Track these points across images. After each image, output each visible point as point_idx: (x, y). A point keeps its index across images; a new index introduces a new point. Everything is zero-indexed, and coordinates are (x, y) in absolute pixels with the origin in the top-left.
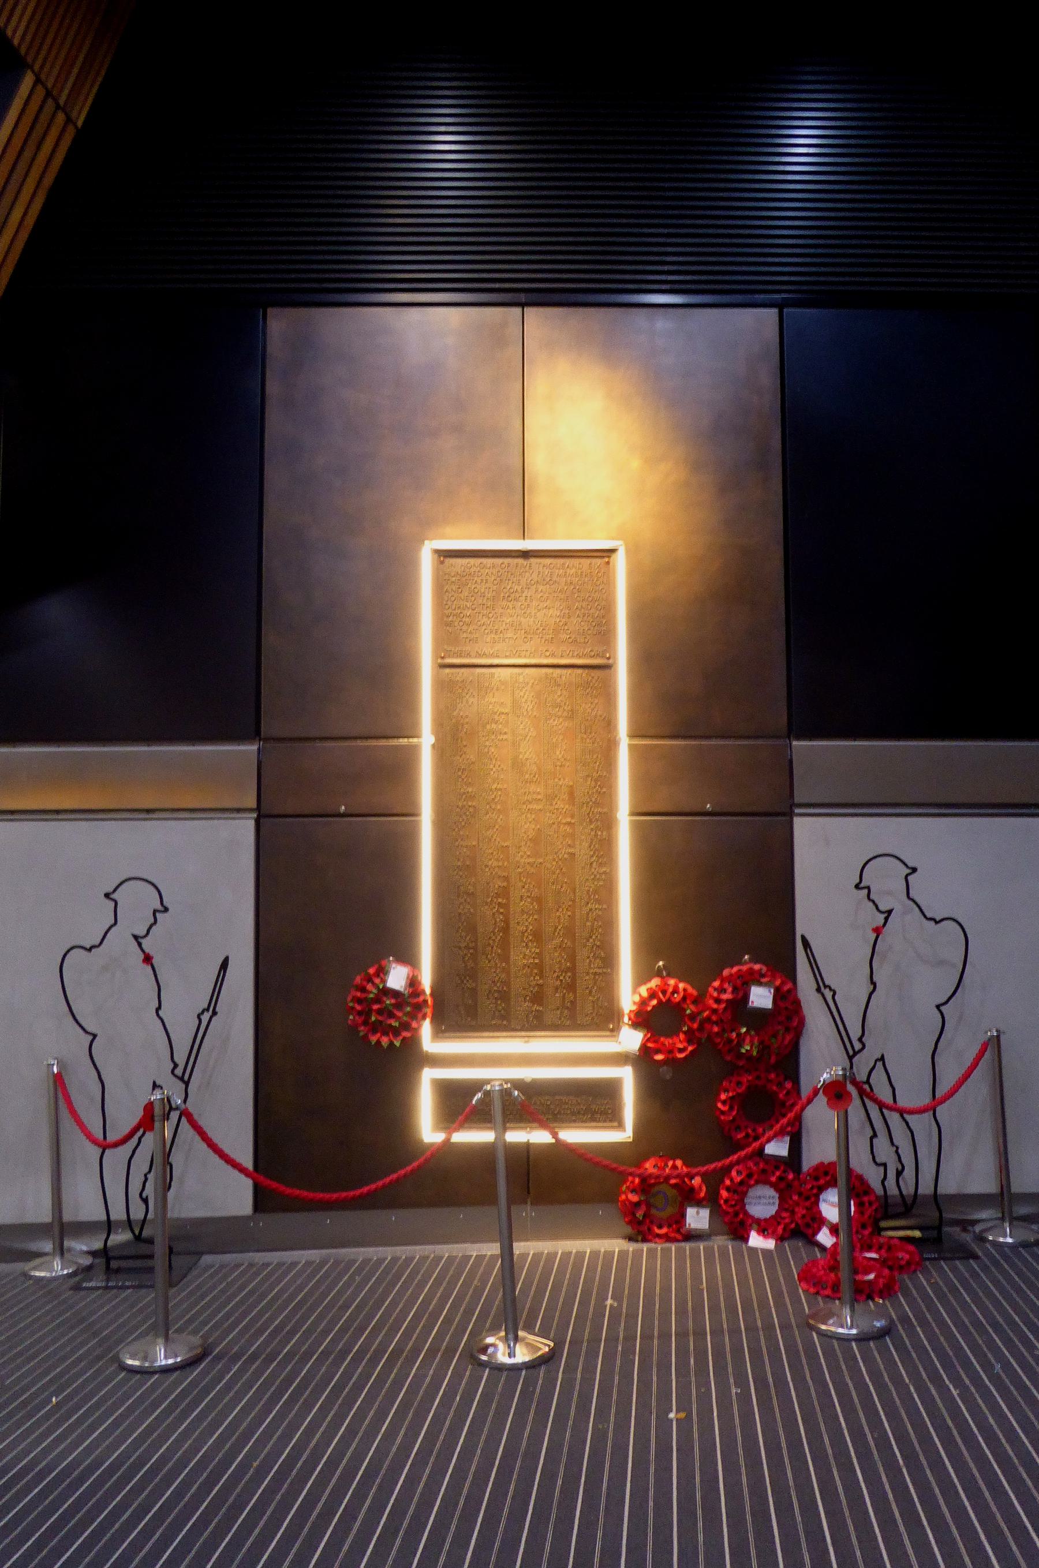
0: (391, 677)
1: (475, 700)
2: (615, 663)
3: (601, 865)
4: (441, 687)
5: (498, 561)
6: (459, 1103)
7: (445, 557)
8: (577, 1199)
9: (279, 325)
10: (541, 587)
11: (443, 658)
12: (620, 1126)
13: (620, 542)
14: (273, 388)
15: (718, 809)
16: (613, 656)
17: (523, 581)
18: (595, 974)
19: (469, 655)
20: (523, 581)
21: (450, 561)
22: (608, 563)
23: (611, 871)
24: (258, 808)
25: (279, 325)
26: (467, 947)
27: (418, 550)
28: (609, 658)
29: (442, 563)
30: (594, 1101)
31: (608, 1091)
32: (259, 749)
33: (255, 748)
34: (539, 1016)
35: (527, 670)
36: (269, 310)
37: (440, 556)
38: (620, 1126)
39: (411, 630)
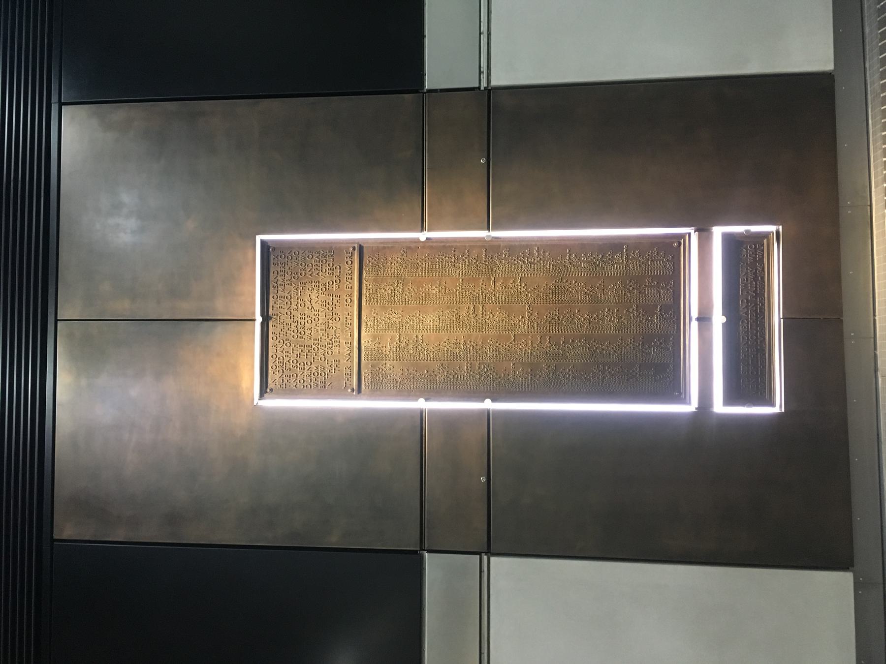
0: (366, 435)
1: (388, 363)
2: (358, 243)
3: (531, 254)
4: (377, 391)
5: (364, 282)
6: (746, 379)
7: (267, 387)
8: (836, 276)
9: (67, 528)
10: (293, 306)
11: (353, 390)
12: (772, 404)
13: (259, 238)
14: (120, 535)
15: (486, 153)
16: (352, 242)
17: (289, 321)
18: (627, 259)
19: (351, 368)
20: (289, 321)
21: (271, 385)
22: (274, 249)
23: (536, 245)
24: (479, 553)
25: (67, 528)
26: (603, 372)
27: (261, 408)
28: (354, 248)
29: (271, 390)
30: (744, 259)
31: (732, 244)
32: (429, 551)
33: (427, 555)
34: (665, 308)
35: (364, 317)
36: (55, 537)
37: (266, 392)
38: (772, 404)
39: (328, 416)
